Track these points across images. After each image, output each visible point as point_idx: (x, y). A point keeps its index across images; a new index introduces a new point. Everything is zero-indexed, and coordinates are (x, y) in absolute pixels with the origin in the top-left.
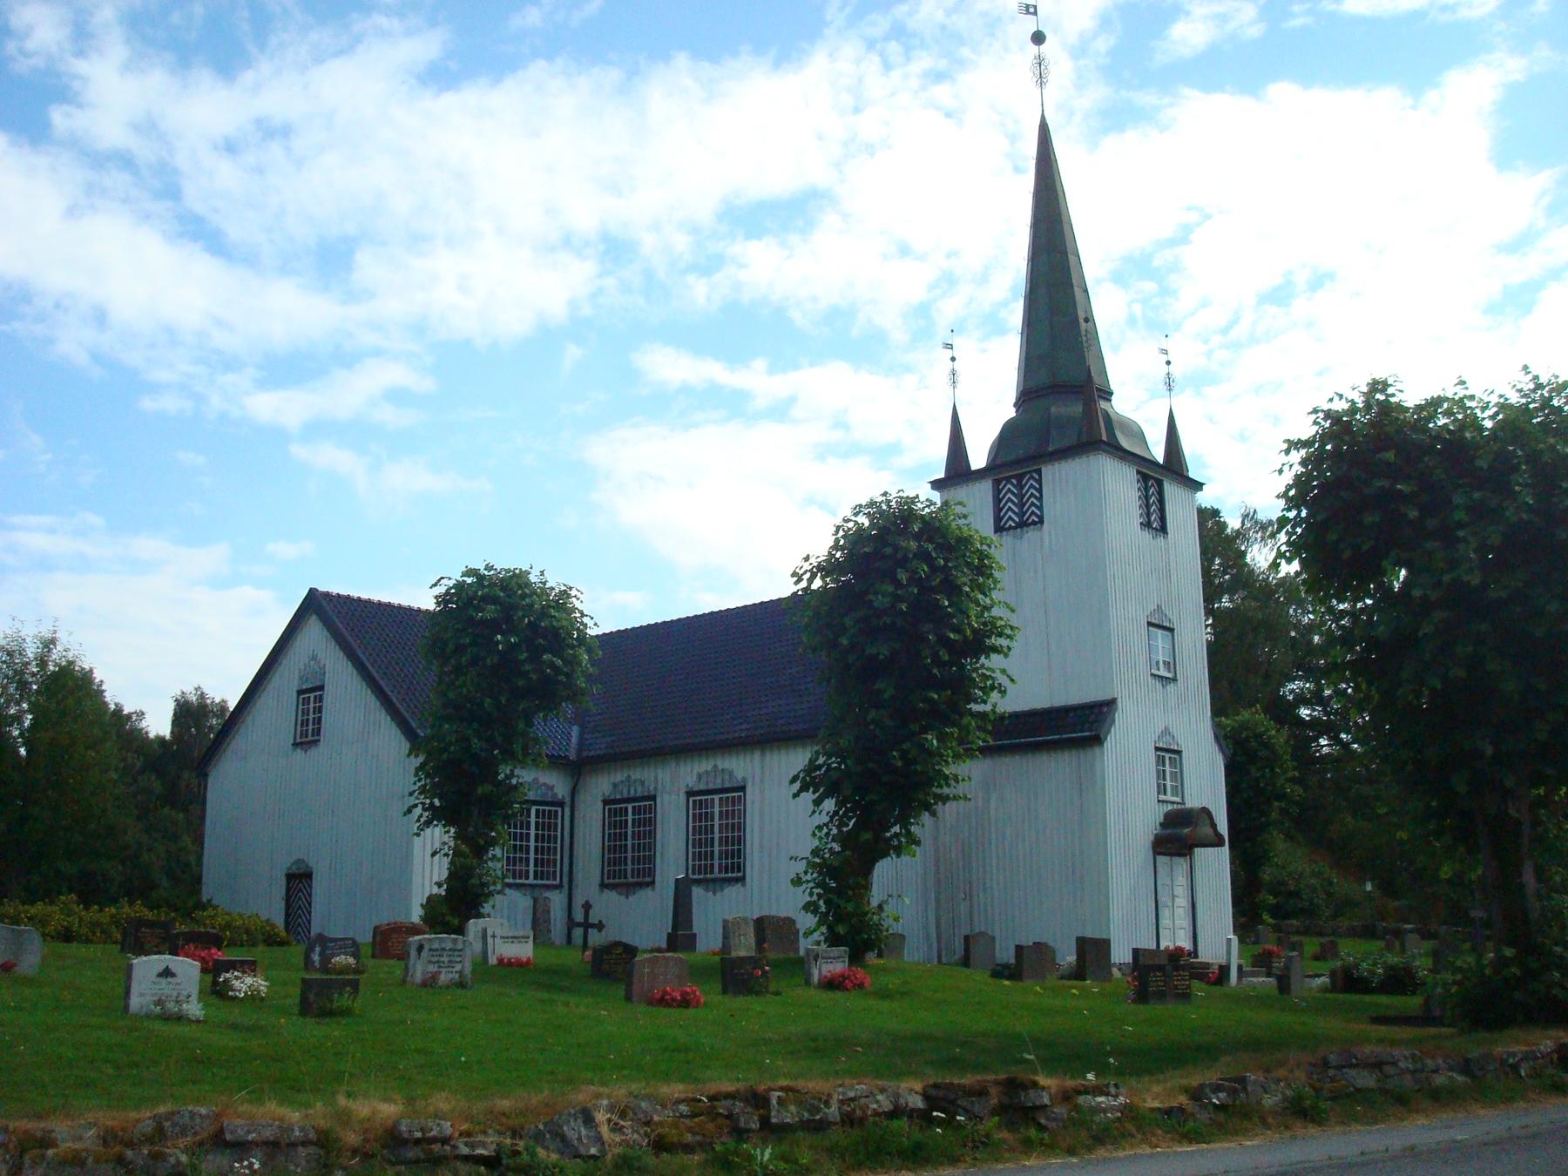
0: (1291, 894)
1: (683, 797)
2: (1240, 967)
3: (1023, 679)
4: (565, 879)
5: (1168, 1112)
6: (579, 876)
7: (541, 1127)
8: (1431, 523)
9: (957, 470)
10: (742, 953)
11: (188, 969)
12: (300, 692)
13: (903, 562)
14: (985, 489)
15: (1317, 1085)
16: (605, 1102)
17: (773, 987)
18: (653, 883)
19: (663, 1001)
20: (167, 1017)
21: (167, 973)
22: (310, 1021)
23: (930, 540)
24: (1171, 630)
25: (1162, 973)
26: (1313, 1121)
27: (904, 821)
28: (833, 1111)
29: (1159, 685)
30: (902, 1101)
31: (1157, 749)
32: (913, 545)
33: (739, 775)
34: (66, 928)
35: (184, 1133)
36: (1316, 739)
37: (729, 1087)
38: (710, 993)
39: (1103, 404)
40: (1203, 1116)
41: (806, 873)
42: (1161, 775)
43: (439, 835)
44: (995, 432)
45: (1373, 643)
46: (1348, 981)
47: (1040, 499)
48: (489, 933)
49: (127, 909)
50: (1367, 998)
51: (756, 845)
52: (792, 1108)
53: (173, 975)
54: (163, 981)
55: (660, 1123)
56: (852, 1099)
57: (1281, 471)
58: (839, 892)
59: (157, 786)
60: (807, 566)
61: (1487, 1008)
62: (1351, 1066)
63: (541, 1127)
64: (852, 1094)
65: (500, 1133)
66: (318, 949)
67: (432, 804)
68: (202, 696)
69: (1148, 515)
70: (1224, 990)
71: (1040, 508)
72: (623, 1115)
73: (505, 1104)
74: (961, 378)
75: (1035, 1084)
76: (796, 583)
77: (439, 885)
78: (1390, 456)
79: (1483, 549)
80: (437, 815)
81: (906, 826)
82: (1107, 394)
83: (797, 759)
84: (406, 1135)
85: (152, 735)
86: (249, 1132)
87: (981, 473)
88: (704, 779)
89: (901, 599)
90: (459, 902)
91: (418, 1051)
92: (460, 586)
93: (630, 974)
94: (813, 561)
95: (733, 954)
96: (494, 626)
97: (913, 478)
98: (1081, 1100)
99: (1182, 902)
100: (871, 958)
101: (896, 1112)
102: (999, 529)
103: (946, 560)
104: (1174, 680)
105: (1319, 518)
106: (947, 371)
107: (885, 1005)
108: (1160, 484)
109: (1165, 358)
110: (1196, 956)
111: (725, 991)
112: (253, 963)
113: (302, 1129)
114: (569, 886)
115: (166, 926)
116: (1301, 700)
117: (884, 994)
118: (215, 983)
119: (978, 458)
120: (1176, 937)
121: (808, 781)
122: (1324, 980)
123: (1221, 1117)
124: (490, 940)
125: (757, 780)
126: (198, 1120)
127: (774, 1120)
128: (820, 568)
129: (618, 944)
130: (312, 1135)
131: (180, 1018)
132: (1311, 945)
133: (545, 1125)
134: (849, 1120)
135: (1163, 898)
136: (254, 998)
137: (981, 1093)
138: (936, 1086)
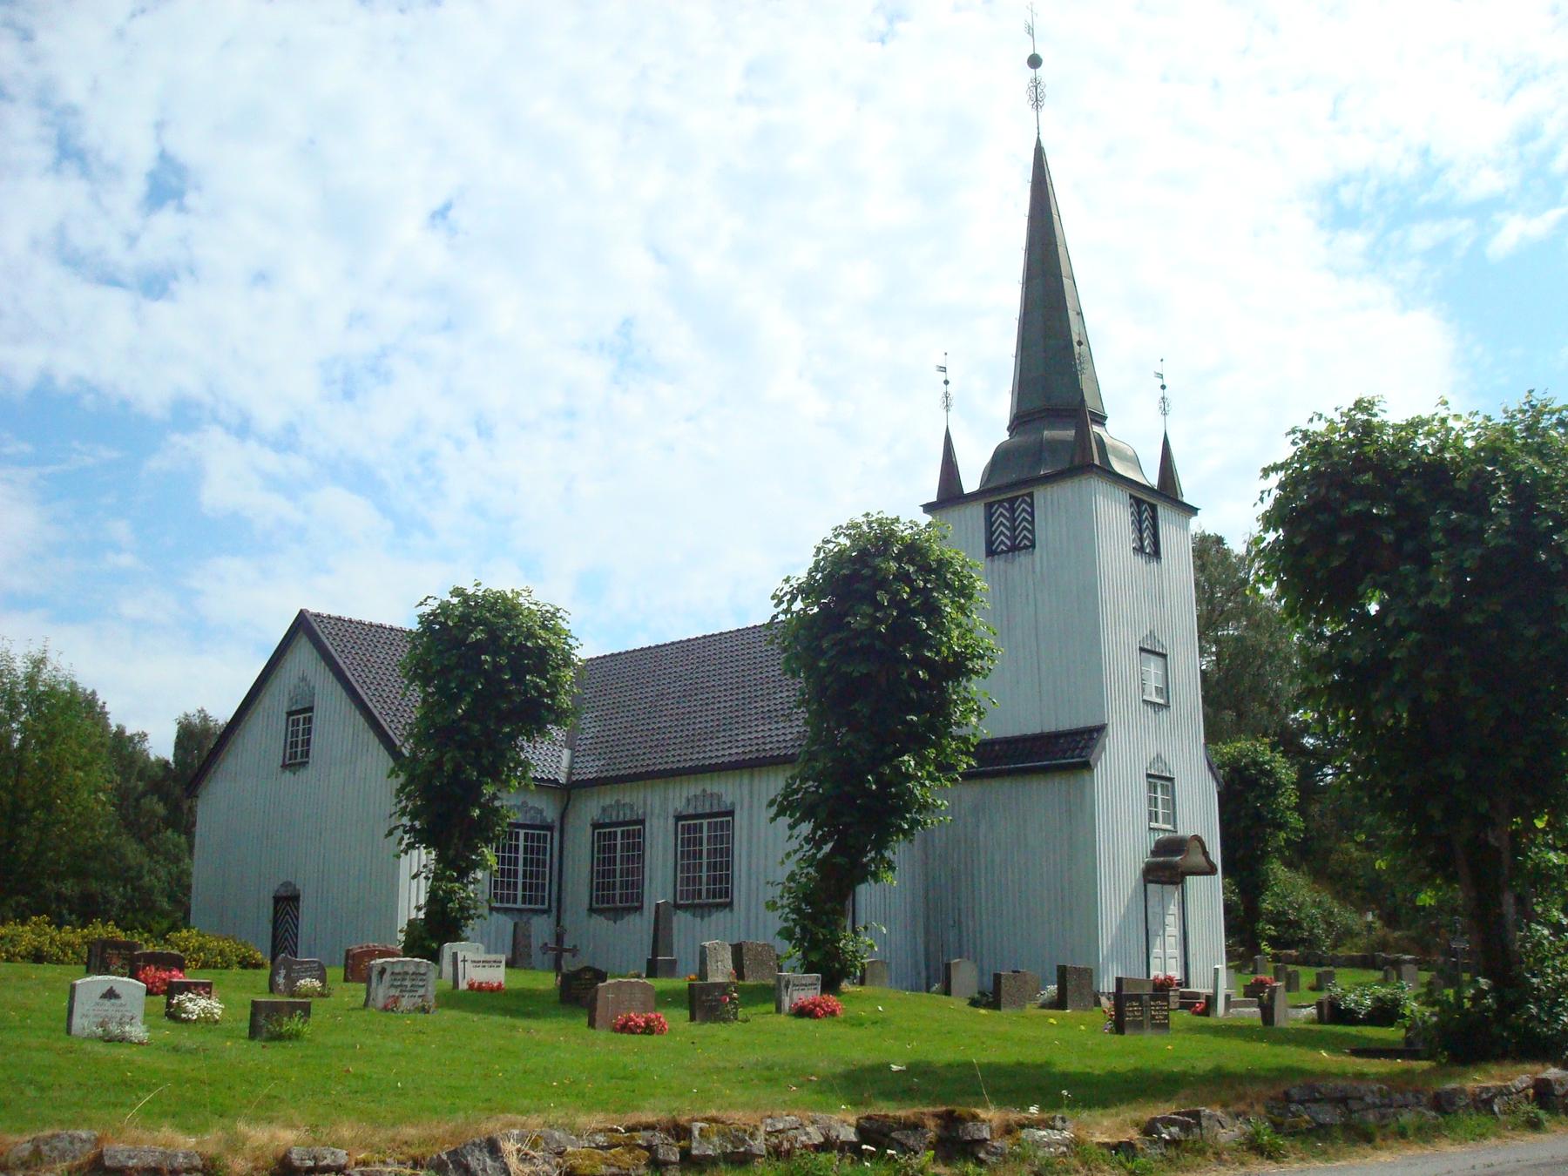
0: (1291, 924)
1: (671, 821)
2: (1228, 997)
3: (996, 706)
4: (554, 904)
5: (1117, 1147)
6: (568, 900)
7: (444, 1157)
8: (1409, 546)
9: (950, 493)
10: (720, 979)
11: (131, 988)
12: (290, 714)
13: (882, 584)
14: (977, 512)
15: (1279, 1120)
16: (516, 1132)
17: (741, 1013)
18: (731, 904)
19: (625, 1028)
20: (109, 1039)
21: (111, 994)
22: (256, 1045)
23: (911, 562)
24: (1164, 656)
25: (1142, 1004)
26: (1270, 1157)
27: (881, 845)
28: (759, 1145)
29: (1150, 711)
30: (833, 1134)
31: (1149, 776)
32: (893, 565)
33: (728, 799)
34: (37, 949)
35: (62, 1157)
36: (1320, 767)
37: (648, 1117)
38: (675, 1018)
39: (1096, 429)
40: (1155, 1152)
41: (782, 897)
42: (1153, 802)
43: (423, 857)
44: (986, 457)
45: (1347, 667)
46: (1335, 1013)
47: (1032, 523)
48: (460, 958)
49: (100, 930)
50: (1353, 1030)
51: (744, 875)
52: (715, 1139)
53: (117, 997)
54: (106, 1001)
55: (573, 1154)
56: (780, 1131)
57: (1262, 499)
58: (813, 918)
59: (160, 809)
60: (787, 588)
61: (1466, 1040)
62: (1316, 1101)
63: (444, 1157)
64: (780, 1126)
65: (401, 1163)
66: (283, 972)
67: (412, 827)
68: (205, 718)
69: (1141, 540)
70: (1210, 1021)
71: (1032, 532)
72: (534, 1145)
73: (409, 1132)
74: (954, 402)
75: (975, 1117)
76: (777, 606)
77: (419, 909)
78: (1367, 477)
79: (1460, 571)
80: (425, 837)
81: (879, 852)
82: (1101, 419)
83: (773, 784)
84: (297, 1163)
85: (153, 758)
86: (130, 1157)
87: (974, 496)
88: (693, 803)
89: (880, 621)
90: (439, 926)
91: (356, 1076)
92: (445, 607)
93: (594, 999)
94: (794, 582)
95: (710, 980)
96: (479, 647)
97: (905, 501)
98: (1024, 1134)
99: (1173, 929)
100: (845, 986)
101: (827, 1145)
102: (991, 552)
103: (926, 582)
104: (1167, 706)
105: (1298, 540)
106: (941, 394)
107: (854, 1033)
108: (1153, 508)
109: (942, 377)
110: (1187, 985)
111: (693, 1018)
112: (209, 985)
113: (186, 1156)
114: (558, 910)
115: (131, 946)
116: (1305, 729)
117: (858, 1023)
118: (169, 1005)
119: (971, 482)
120: (1165, 965)
121: (785, 806)
122: (1313, 1011)
123: (1172, 1152)
124: (460, 965)
125: (746, 805)
126: (78, 1145)
127: (694, 1152)
128: (800, 590)
129: (587, 969)
130: (198, 1162)
131: (122, 1039)
132: (1307, 975)
133: (448, 1154)
134: (776, 1153)
135: (1152, 927)
136: (208, 1021)
137: (915, 1126)
138: (869, 1118)
